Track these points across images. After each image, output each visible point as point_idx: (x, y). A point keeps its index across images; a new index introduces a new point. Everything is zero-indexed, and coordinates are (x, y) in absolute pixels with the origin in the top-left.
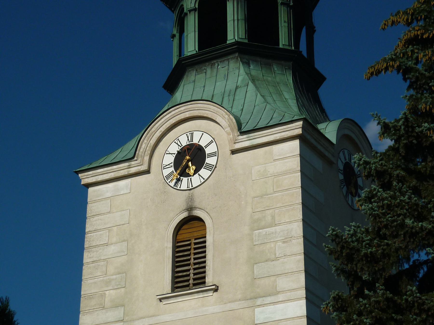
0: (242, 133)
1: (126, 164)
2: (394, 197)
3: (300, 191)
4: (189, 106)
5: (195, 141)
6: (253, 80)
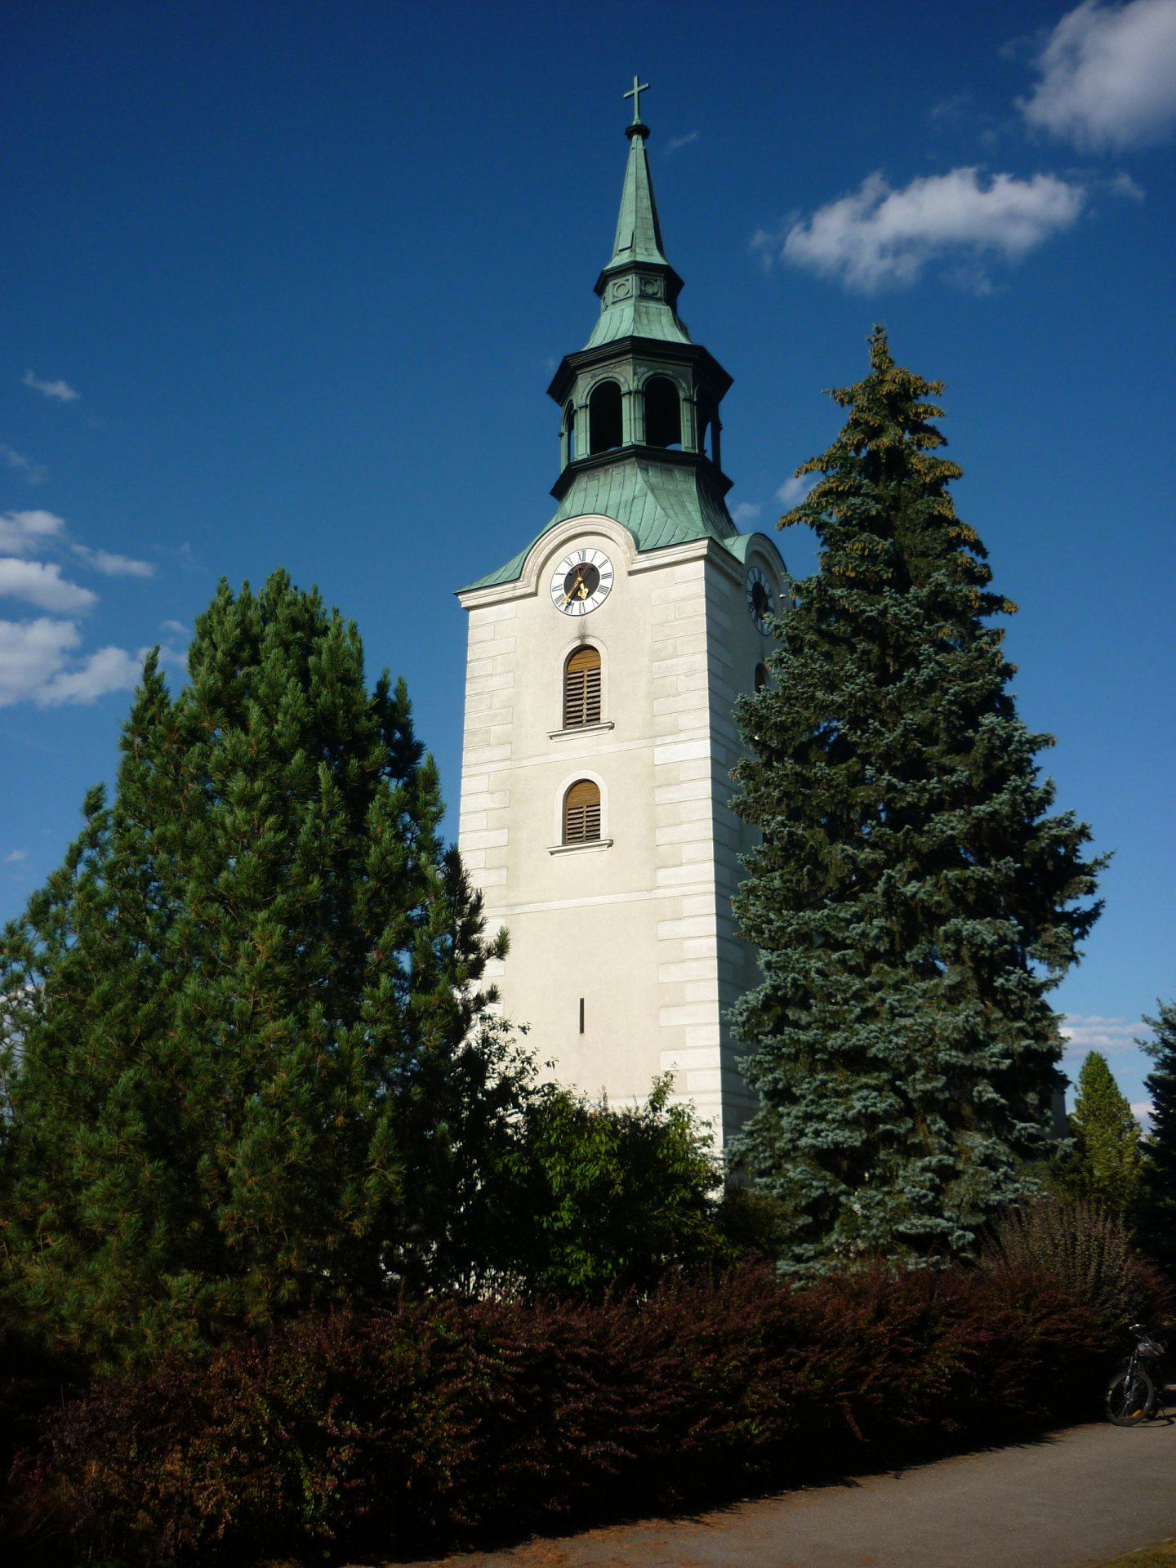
0: (641, 552)
1: (511, 585)
2: (805, 665)
3: (704, 618)
4: (580, 520)
5: (588, 560)
6: (652, 489)
